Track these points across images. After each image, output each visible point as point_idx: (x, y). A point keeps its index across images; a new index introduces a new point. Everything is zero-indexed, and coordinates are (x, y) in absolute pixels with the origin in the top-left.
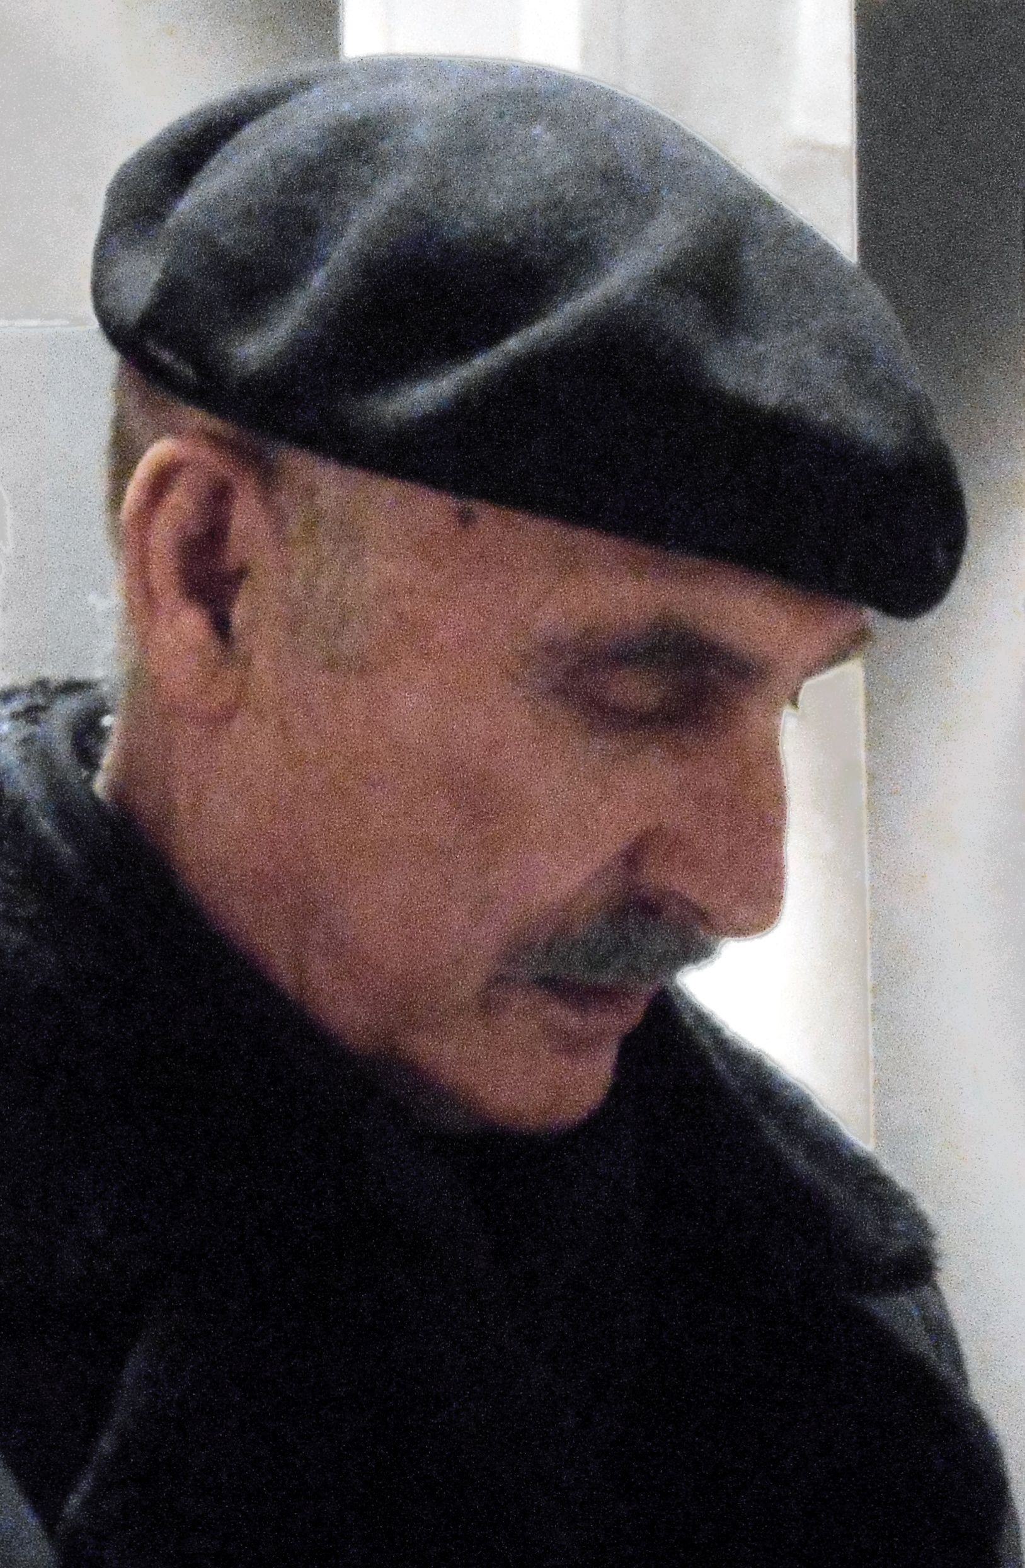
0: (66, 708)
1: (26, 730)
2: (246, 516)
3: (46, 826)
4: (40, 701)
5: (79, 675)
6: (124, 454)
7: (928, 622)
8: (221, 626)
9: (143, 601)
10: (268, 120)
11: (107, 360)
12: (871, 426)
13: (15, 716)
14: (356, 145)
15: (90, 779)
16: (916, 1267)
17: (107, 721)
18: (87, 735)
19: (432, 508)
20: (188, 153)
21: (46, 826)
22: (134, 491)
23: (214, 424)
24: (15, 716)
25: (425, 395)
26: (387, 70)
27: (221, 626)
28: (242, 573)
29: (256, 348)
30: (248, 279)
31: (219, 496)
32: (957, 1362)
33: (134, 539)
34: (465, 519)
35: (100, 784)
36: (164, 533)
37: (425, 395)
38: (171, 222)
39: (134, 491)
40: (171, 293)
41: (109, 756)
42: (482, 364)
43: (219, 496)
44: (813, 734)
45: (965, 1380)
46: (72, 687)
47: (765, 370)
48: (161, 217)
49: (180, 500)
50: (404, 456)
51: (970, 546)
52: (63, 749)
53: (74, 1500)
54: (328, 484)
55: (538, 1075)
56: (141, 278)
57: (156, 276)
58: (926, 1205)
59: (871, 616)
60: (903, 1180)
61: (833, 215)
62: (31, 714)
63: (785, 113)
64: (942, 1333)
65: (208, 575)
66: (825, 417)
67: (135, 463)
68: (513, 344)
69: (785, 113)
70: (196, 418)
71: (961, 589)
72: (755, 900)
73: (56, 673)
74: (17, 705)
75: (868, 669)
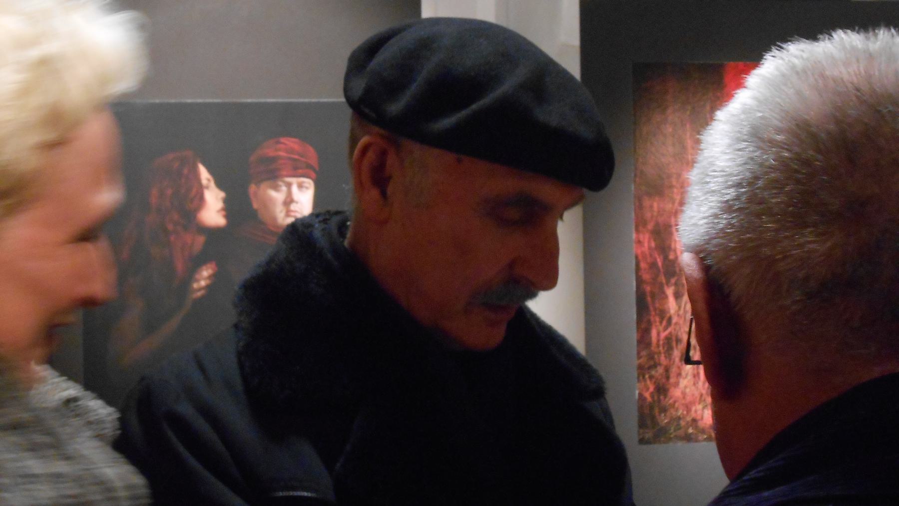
0: (335, 220)
1: (323, 226)
2: (391, 160)
3: (329, 256)
4: (328, 217)
5: (340, 209)
6: (354, 140)
7: (602, 193)
8: (384, 194)
9: (360, 185)
10: (398, 37)
11: (349, 111)
12: (585, 132)
13: (320, 222)
14: (425, 45)
15: (343, 241)
16: (599, 392)
17: (349, 223)
18: (342, 228)
19: (449, 158)
20: (372, 48)
21: (329, 256)
22: (356, 152)
23: (382, 131)
24: (320, 222)
25: (446, 122)
26: (435, 22)
27: (384, 194)
28: (390, 177)
29: (395, 108)
30: (391, 86)
31: (383, 154)
32: (612, 422)
33: (357, 168)
34: (459, 161)
35: (346, 243)
36: (366, 162)
37: (446, 122)
38: (368, 69)
39: (356, 152)
40: (368, 90)
41: (349, 235)
42: (464, 113)
43: (383, 154)
44: (568, 230)
45: (614, 428)
46: (337, 213)
47: (552, 115)
48: (364, 67)
49: (371, 155)
50: (443, 141)
51: (616, 169)
52: (335, 231)
53: (338, 465)
54: (416, 151)
55: (482, 333)
56: (359, 86)
57: (363, 85)
58: (602, 374)
59: (585, 191)
60: (595, 366)
61: (573, 66)
62: (325, 221)
63: (560, 37)
64: (607, 413)
65: (379, 178)
66: (571, 129)
67: (357, 144)
68: (474, 107)
69: (560, 37)
70: (376, 129)
71: (613, 183)
72: (549, 280)
73: (332, 208)
74: (321, 218)
75: (585, 212)
